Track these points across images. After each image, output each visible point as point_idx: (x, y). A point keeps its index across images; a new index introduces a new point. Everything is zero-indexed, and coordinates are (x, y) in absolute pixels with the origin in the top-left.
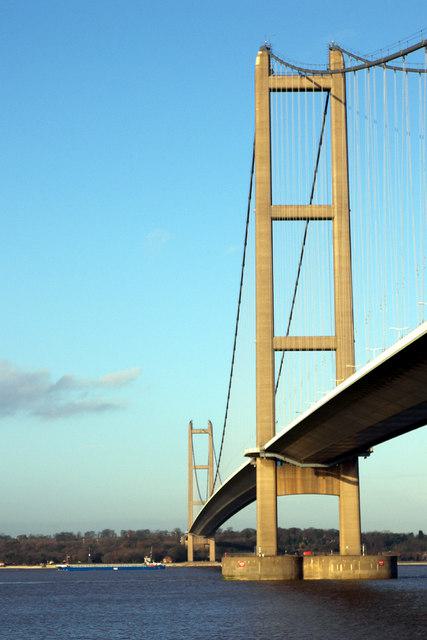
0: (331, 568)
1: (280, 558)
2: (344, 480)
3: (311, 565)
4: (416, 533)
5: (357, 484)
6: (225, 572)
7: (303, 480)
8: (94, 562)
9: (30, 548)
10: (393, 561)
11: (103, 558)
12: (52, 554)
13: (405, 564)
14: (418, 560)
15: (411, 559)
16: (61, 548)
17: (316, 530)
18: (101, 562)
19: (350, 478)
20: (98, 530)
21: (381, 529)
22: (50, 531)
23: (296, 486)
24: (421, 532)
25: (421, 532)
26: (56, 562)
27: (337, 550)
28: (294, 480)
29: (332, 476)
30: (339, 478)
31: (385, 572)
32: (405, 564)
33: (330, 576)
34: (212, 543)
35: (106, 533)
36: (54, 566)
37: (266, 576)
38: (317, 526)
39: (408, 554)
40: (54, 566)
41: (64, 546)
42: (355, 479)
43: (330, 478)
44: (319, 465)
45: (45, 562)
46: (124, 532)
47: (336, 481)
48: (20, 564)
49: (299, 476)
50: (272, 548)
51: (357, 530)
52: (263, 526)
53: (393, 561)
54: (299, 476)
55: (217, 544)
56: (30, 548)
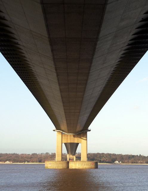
0: (77, 165)
1: (62, 162)
2: (82, 139)
3: (72, 164)
4: (139, 155)
5: (87, 140)
6: (46, 166)
7: (70, 139)
8: (39, 162)
9: (22, 158)
10: (96, 163)
11: (42, 161)
12: (27, 160)
13: (102, 164)
14: (137, 163)
15: (135, 163)
16: (31, 158)
17: (109, 154)
18: (41, 162)
19: (84, 138)
20: (45, 152)
21: (95, 152)
22: (31, 153)
23: (68, 140)
24: (140, 155)
25: (140, 155)
26: (28, 162)
27: (81, 160)
28: (68, 138)
29: (79, 137)
30: (81, 138)
31: (93, 166)
32: (102, 164)
33: (77, 168)
34: (75, 157)
35: (47, 153)
36: (27, 163)
37: (57, 167)
38: (109, 153)
39: (134, 161)
40: (27, 163)
41: (15, 158)
42: (86, 139)
43: (78, 138)
44: (71, 134)
45: (25, 162)
46: (52, 153)
47: (80, 139)
48: (17, 162)
49: (69, 137)
50: (60, 159)
51: (86, 152)
52: (57, 152)
53: (96, 163)
54: (69, 137)
55: (76, 157)
56: (22, 158)
